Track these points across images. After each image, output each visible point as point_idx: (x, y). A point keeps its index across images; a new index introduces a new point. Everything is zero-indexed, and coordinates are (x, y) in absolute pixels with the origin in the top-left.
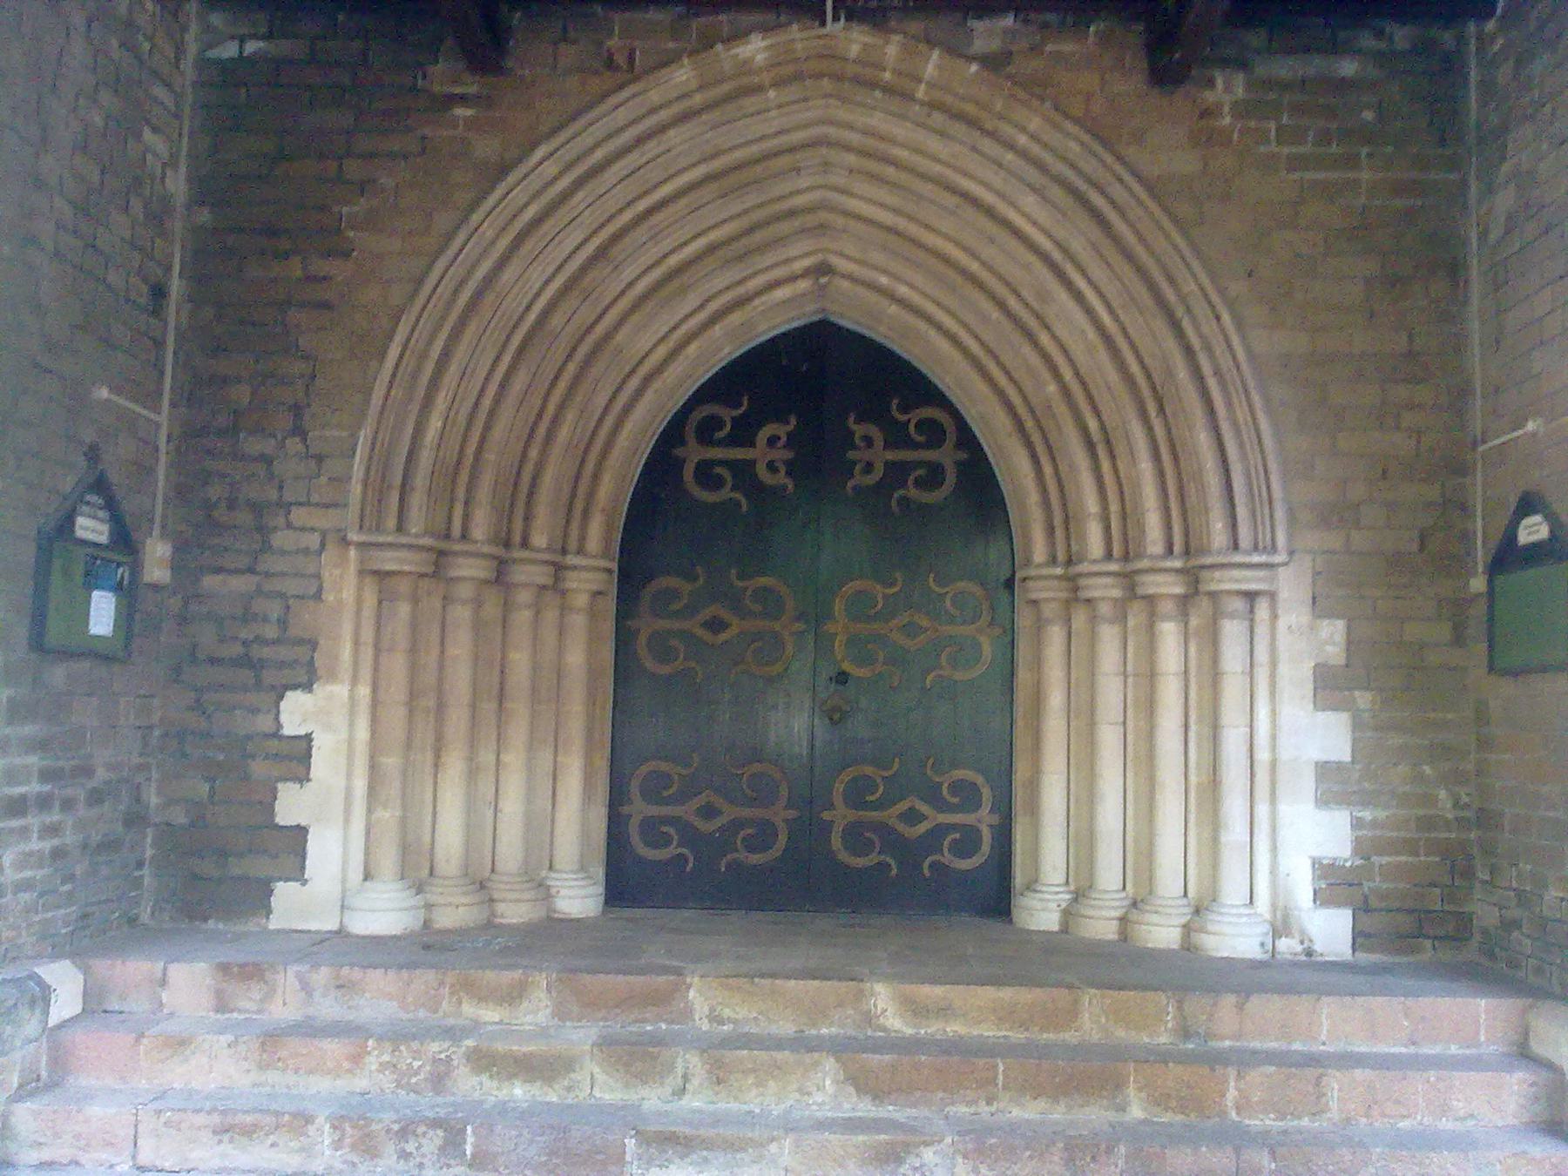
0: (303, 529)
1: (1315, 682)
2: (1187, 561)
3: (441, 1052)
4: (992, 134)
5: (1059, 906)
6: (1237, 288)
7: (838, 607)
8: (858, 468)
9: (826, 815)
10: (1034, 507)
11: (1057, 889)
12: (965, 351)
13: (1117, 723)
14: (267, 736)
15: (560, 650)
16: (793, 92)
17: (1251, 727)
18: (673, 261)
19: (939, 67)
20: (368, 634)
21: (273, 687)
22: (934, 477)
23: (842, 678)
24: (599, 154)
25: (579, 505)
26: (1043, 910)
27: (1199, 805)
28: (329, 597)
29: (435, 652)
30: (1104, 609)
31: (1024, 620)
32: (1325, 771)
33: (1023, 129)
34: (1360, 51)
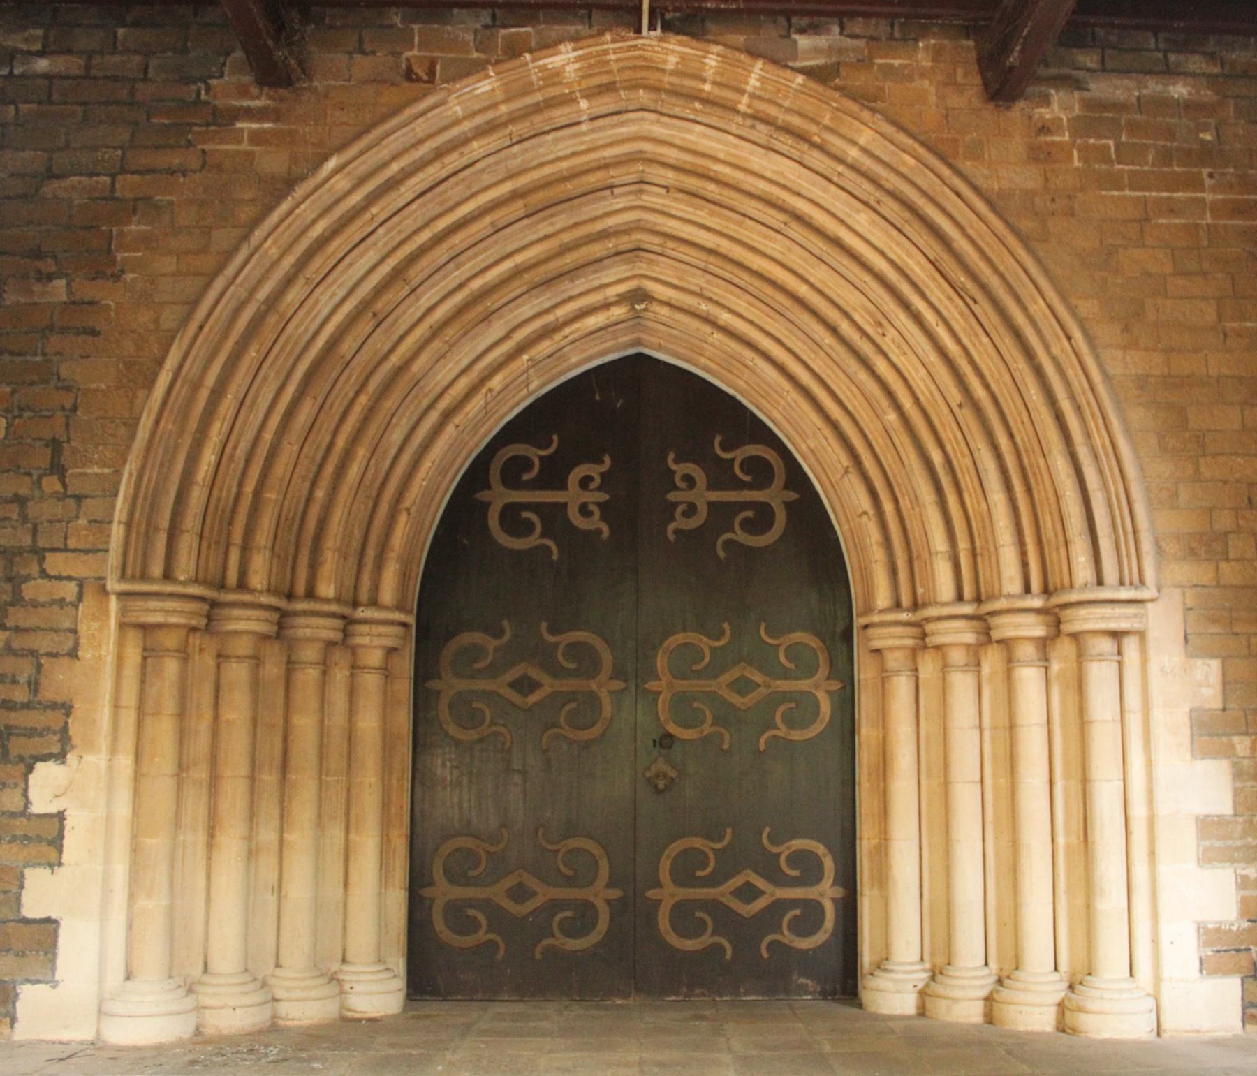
0: (59, 578)
1: (1192, 727)
2: (1048, 600)
4: (821, 148)
6: (1088, 307)
7: (661, 662)
8: (680, 509)
9: (650, 894)
10: (875, 547)
11: (909, 968)
12: (792, 378)
13: (973, 782)
14: (13, 815)
15: (352, 712)
16: (606, 103)
17: (1124, 780)
18: (476, 284)
19: (762, 79)
20: (130, 695)
21: (21, 759)
22: (762, 518)
23: (665, 741)
24: (395, 167)
25: (371, 553)
26: (899, 992)
27: (1069, 870)
28: (86, 653)
29: (208, 715)
30: (957, 657)
31: (865, 672)
32: (1207, 825)
33: (854, 143)
34: (1186, 74)
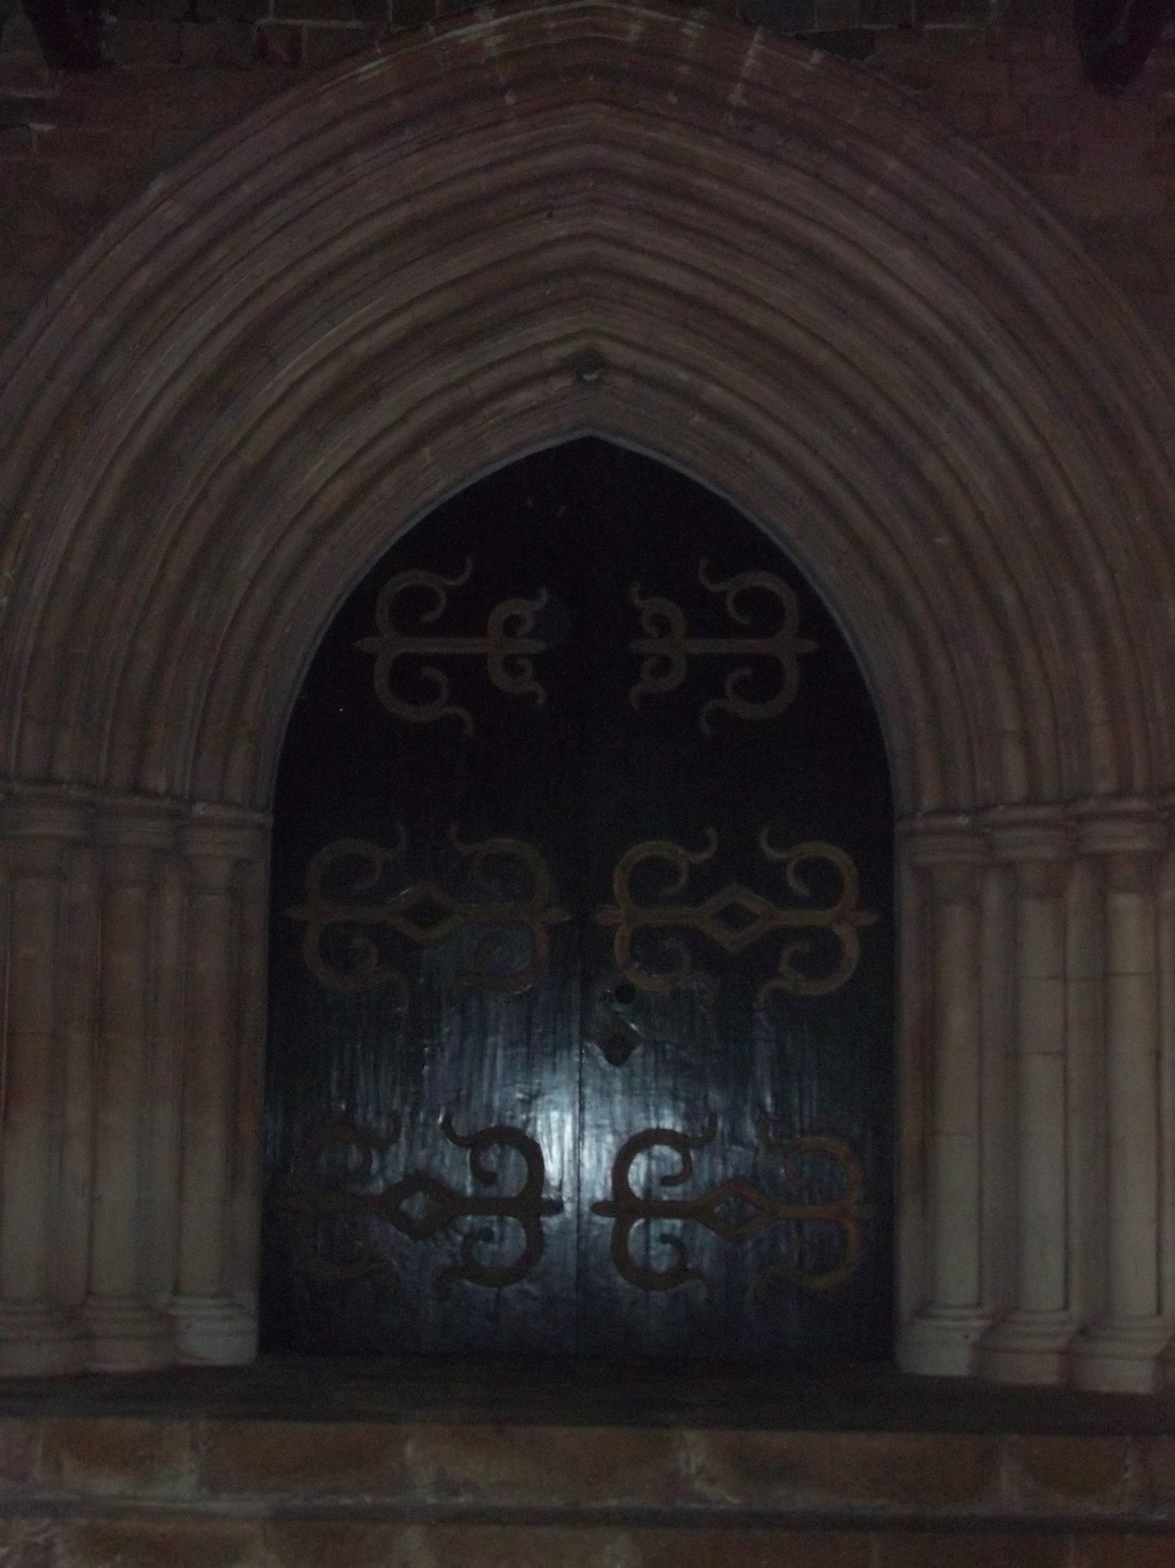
3: (35, 1534)
5: (966, 1337)
11: (966, 1312)
31: (908, 898)
